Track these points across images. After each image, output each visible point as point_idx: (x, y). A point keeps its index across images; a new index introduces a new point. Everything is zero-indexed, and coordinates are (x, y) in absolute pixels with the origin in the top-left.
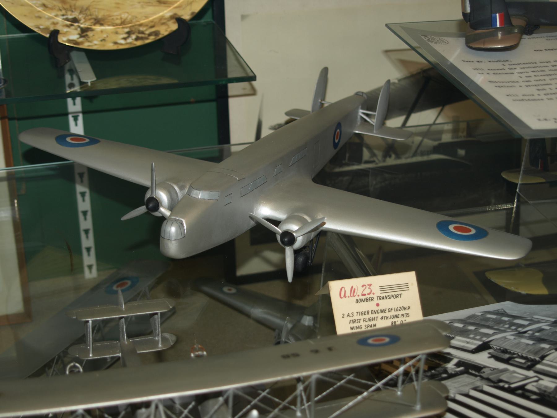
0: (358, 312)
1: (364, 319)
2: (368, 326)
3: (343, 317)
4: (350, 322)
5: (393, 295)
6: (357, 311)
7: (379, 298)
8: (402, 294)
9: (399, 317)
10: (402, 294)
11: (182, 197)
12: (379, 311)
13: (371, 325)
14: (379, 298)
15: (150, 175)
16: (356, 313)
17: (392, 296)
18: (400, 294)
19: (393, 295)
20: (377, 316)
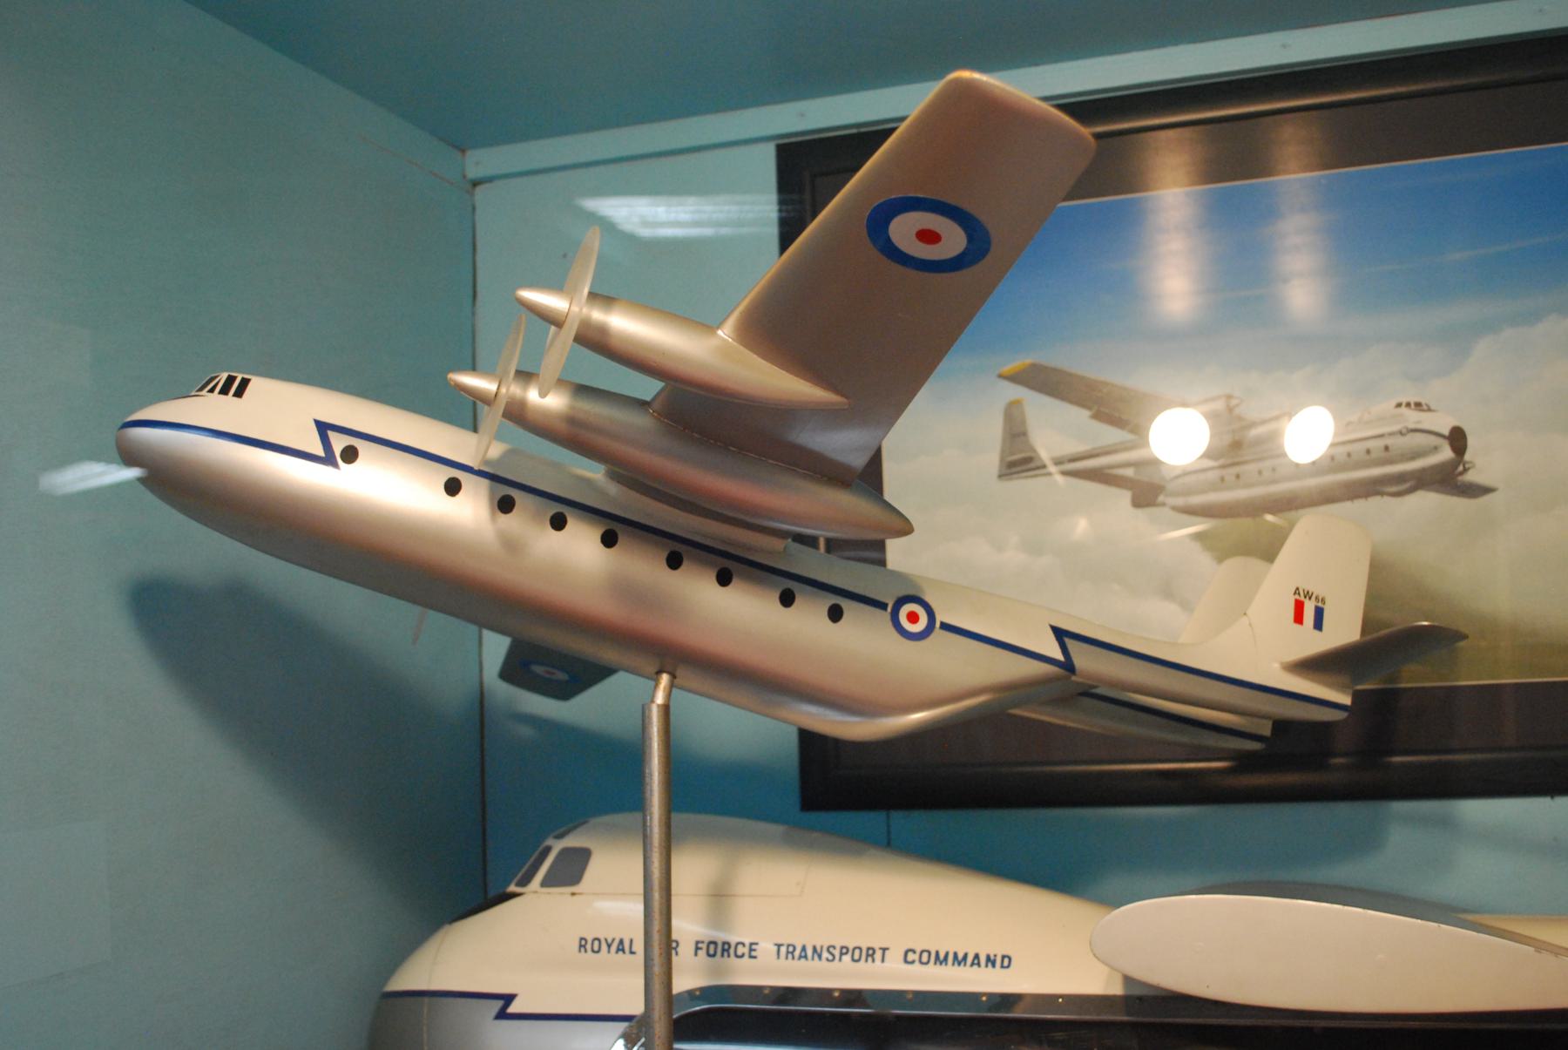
0: (782, 945)
1: (697, 943)
2: (844, 951)
3: (884, 950)
4: (697, 949)
5: (851, 948)
6: (780, 942)
7: (783, 949)
8: (888, 949)
9: (753, 954)
10: (888, 949)
11: (1301, 512)
12: (740, 950)
13: (977, 956)
14: (783, 949)
15: (672, 718)
16: (776, 948)
17: (844, 951)
18: (881, 949)
19: (851, 948)
20: (884, 946)
